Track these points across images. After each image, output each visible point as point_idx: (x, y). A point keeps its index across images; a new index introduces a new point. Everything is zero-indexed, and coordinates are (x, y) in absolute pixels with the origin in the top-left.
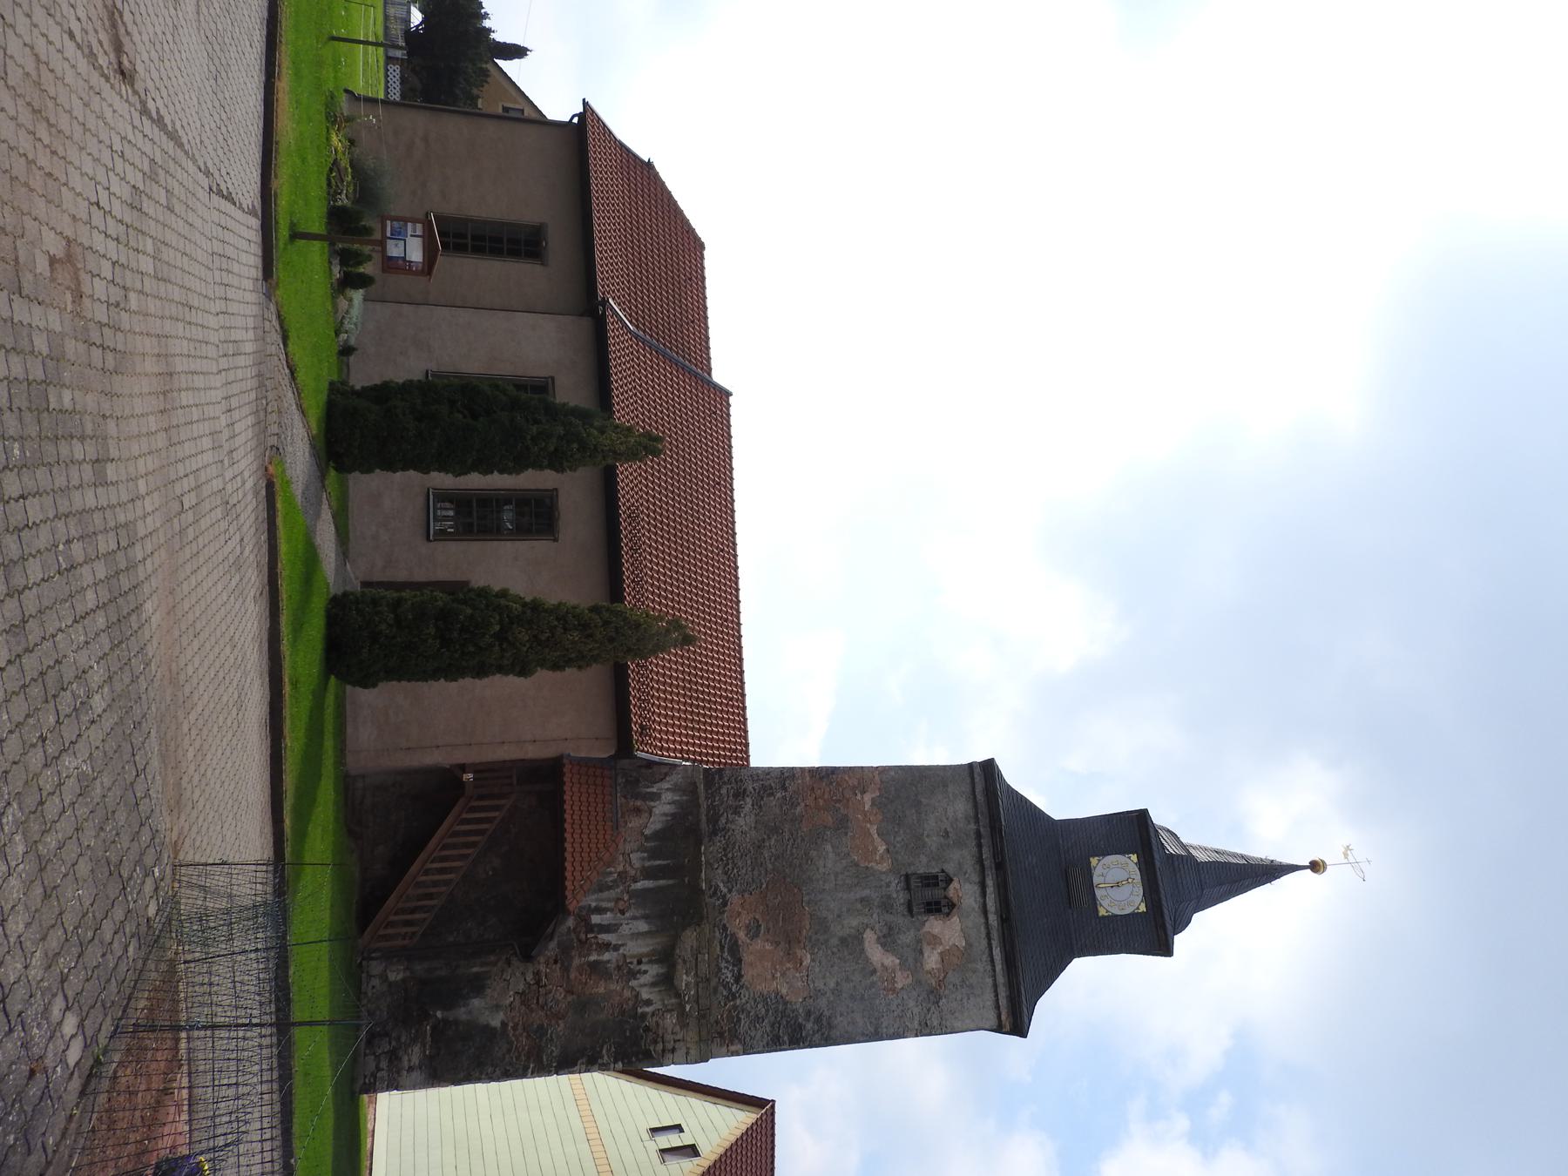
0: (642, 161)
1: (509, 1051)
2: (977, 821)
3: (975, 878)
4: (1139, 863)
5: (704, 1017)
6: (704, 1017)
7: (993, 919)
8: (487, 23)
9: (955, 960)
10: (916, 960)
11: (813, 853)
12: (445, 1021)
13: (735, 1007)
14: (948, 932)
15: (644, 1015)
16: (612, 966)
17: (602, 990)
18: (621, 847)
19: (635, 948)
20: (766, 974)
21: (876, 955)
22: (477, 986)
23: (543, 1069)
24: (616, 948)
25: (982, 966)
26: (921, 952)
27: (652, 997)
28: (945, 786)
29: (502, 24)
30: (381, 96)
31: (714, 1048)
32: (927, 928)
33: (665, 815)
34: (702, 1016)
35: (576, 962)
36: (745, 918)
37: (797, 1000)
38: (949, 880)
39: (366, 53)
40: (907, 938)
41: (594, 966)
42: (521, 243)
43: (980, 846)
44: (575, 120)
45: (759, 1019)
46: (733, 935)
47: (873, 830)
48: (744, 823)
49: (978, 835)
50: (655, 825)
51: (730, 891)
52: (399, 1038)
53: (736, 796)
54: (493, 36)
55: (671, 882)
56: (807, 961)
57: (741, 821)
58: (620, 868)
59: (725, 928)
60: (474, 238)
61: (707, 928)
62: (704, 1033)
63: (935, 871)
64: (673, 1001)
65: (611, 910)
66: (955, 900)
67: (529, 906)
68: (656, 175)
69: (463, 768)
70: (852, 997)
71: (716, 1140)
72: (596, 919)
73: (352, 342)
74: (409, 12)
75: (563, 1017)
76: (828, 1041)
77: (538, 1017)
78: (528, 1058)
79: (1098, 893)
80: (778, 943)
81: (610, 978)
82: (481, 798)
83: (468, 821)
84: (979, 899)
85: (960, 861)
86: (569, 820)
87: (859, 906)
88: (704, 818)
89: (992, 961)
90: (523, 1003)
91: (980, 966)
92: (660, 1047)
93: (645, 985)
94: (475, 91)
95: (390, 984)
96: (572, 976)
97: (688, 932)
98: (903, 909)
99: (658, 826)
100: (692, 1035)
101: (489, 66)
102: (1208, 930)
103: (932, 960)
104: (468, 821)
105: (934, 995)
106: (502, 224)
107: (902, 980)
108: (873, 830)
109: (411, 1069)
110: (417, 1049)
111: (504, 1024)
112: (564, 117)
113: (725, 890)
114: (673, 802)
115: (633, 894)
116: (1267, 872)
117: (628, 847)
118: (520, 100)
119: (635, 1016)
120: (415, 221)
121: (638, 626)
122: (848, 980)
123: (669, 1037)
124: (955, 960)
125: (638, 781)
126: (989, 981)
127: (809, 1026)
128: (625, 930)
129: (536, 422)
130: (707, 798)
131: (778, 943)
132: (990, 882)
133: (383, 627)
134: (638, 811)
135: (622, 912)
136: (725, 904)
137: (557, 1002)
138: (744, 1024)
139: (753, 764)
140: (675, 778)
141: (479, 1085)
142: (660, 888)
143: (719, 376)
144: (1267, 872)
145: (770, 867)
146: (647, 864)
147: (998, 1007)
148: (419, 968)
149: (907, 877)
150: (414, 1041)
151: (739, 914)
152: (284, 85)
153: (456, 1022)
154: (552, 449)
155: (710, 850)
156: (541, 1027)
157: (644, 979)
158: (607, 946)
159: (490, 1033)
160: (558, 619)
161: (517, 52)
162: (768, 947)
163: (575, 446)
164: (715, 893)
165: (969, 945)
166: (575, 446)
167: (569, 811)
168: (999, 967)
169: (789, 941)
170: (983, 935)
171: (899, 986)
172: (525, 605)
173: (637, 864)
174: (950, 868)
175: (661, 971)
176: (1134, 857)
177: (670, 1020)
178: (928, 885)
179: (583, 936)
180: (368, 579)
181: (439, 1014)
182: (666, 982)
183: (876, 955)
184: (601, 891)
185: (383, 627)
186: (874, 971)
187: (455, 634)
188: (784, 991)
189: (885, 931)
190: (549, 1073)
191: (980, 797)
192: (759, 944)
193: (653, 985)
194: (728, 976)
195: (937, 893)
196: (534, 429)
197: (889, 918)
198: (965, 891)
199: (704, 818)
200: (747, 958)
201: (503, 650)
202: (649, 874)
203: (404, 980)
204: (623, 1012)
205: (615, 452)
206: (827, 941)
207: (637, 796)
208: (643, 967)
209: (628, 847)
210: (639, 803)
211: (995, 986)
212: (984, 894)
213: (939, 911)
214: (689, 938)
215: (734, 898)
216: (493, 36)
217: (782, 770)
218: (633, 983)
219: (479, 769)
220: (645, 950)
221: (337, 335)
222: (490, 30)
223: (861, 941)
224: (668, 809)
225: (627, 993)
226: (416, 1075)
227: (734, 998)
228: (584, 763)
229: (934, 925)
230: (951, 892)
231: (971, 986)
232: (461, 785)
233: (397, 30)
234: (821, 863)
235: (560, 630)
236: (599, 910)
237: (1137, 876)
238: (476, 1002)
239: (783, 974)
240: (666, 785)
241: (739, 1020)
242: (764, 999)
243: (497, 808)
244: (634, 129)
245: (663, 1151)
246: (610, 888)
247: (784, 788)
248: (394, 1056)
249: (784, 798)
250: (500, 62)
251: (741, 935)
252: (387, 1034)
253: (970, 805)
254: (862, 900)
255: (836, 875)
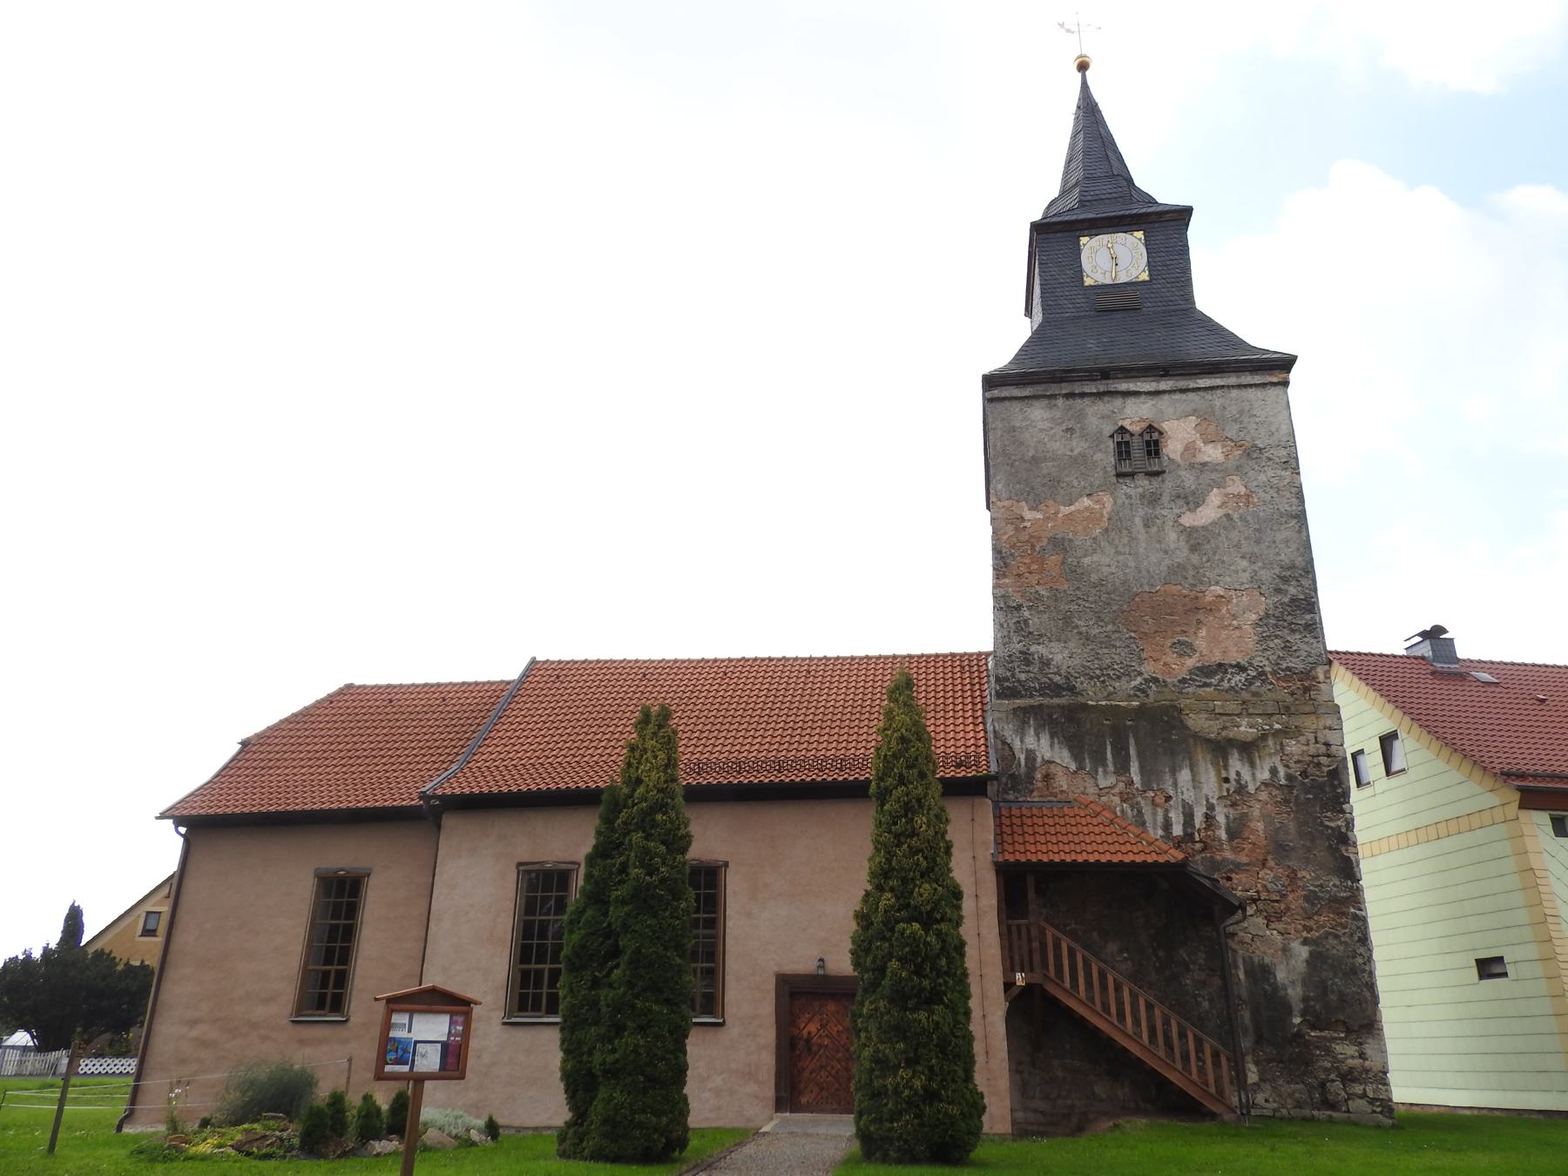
0: (239, 753)
1: (1336, 937)
2: (1053, 397)
3: (1118, 402)
4: (1091, 236)
5: (1287, 708)
6: (1287, 708)
7: (1164, 385)
8: (37, 954)
9: (1212, 428)
10: (1214, 470)
11: (1094, 577)
12: (1303, 1014)
13: (1274, 673)
14: (1179, 434)
15: (1289, 777)
16: (1232, 813)
17: (1260, 826)
18: (1091, 798)
19: (1210, 784)
20: (1233, 638)
21: (1208, 513)
22: (1260, 973)
23: (1355, 898)
24: (1211, 807)
25: (1217, 399)
26: (1204, 464)
27: (1267, 768)
28: (1014, 429)
29: (39, 935)
30: (130, 1081)
31: (1322, 698)
32: (1176, 457)
33: (1052, 745)
34: (1287, 710)
35: (1229, 855)
36: (1171, 658)
37: (1263, 604)
38: (1122, 430)
39: (76, 1101)
40: (1189, 480)
41: (1233, 834)
42: (340, 900)
43: (1083, 395)
44: (183, 830)
45: (1287, 647)
46: (1190, 672)
47: (1065, 510)
48: (1061, 655)
49: (1070, 396)
50: (1063, 757)
51: (1140, 674)
52: (1326, 1070)
53: (1028, 662)
54: (53, 946)
55: (1132, 741)
56: (1219, 590)
57: (1058, 658)
58: (1117, 800)
59: (1183, 681)
60: (328, 961)
61: (1183, 703)
62: (1307, 709)
63: (1111, 445)
64: (1270, 742)
65: (1167, 811)
66: (1144, 425)
67: (1173, 905)
68: (259, 736)
69: (1009, 985)
70: (1258, 542)
71: (1375, 713)
72: (1177, 830)
73: (481, 1123)
74: (13, 1047)
75: (1294, 871)
76: (1308, 570)
77: (1295, 901)
78: (1344, 914)
79: (1123, 279)
80: (1199, 622)
81: (1244, 815)
82: (1045, 965)
83: (1074, 979)
84: (1143, 398)
85: (1106, 416)
86: (1096, 856)
87: (1154, 530)
88: (1056, 701)
89: (1212, 388)
90: (1279, 920)
91: (1218, 403)
92: (1324, 760)
93: (1256, 775)
94: (120, 968)
95: (1262, 1080)
96: (1244, 860)
97: (1190, 723)
98: (1156, 482)
99: (1066, 753)
100: (1309, 723)
101: (91, 950)
102: (1157, 179)
103: (1213, 453)
104: (1074, 979)
105: (1252, 452)
106: (313, 925)
107: (1236, 486)
108: (1065, 510)
109: (1362, 1056)
110: (1338, 1048)
111: (1305, 942)
112: (178, 843)
113: (1139, 679)
114: (1037, 735)
115: (1147, 786)
116: (1089, 112)
117: (1092, 790)
118: (136, 913)
119: (1290, 787)
120: (387, 1025)
121: (903, 739)
122: (1238, 546)
123: (1312, 749)
124: (1212, 428)
125: (1012, 776)
126: (1234, 393)
127: (1292, 590)
128: (1189, 796)
129: (624, 869)
130: (1031, 696)
131: (1199, 622)
132: (1123, 386)
133: (917, 1084)
134: (1047, 777)
135: (1168, 798)
136: (1156, 680)
137: (1277, 878)
138: (1296, 664)
139: (988, 646)
140: (1009, 732)
141: (1378, 973)
142: (1140, 755)
143: (512, 672)
144: (1089, 112)
145: (1110, 627)
146: (1111, 768)
147: (1264, 385)
148: (1246, 1043)
149: (1119, 475)
150: (1329, 1051)
151: (1165, 664)
153: (1305, 999)
154: (663, 848)
155: (1093, 696)
156: (1306, 898)
157: (1246, 775)
158: (1209, 818)
159: (1317, 959)
160: (899, 845)
161: (74, 920)
162: (1203, 632)
163: (659, 817)
164: (1143, 691)
165: (1194, 412)
166: (659, 817)
167: (1063, 856)
168: (1218, 382)
169: (1196, 609)
170: (1183, 396)
171: (1243, 490)
172: (880, 888)
173: (1112, 780)
174: (1109, 429)
175: (1236, 755)
176: (1084, 240)
177: (1293, 747)
178: (1128, 453)
179: (1198, 846)
180: (772, 1102)
181: (1297, 1020)
182: (1248, 749)
183: (1208, 513)
184: (1144, 823)
185: (917, 1084)
186: (1228, 516)
187: (926, 983)
188: (1254, 617)
189: (1181, 502)
190: (1359, 890)
191: (1027, 392)
192: (1201, 640)
193: (1252, 765)
194: (1239, 679)
195: (1136, 444)
196: (635, 872)
197: (1165, 499)
198: (1135, 414)
199: (1056, 701)
200: (1217, 657)
201: (942, 919)
202: (1122, 768)
203: (1257, 1063)
204: (1286, 801)
205: (667, 766)
206: (1195, 567)
207: (1030, 777)
208: (1233, 776)
209: (1092, 790)
210: (1038, 776)
211: (1240, 386)
212: (1136, 394)
213: (1156, 443)
214: (1197, 722)
215: (1149, 669)
216: (53, 946)
217: (997, 609)
218: (1251, 788)
219: (1010, 967)
220: (1212, 773)
221: (474, 1144)
222: (46, 950)
223: (1194, 529)
224: (1045, 740)
225: (1264, 796)
226: (1369, 1049)
227: (1263, 673)
228: (1000, 842)
229: (1173, 448)
230: (1135, 429)
231: (1241, 412)
232: (1029, 988)
233: (35, 1061)
234: (1105, 570)
235: (914, 842)
236: (1167, 826)
237: (1104, 238)
238: (1281, 975)
239: (1234, 617)
240: (1017, 744)
241: (1288, 669)
242: (1264, 639)
243: (1057, 946)
244: (197, 760)
245: (1388, 772)
246: (1140, 812)
247: (1019, 608)
248: (1348, 1077)
249: (1030, 608)
250: (85, 939)
251: (1190, 662)
252: (1323, 1085)
253: (1036, 403)
254: (1146, 526)
255: (1117, 553)
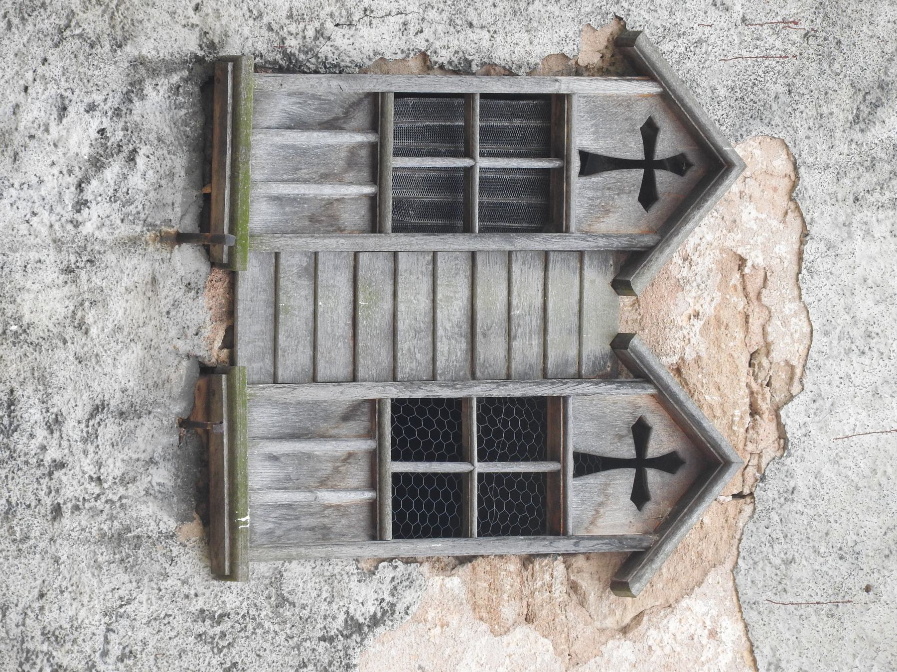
38: (686, 170)
66: (721, 409)
98: (139, 468)
149: (212, 86)
152: (577, 290)
168: (226, 508)
178: (445, 209)
213: (529, 512)
